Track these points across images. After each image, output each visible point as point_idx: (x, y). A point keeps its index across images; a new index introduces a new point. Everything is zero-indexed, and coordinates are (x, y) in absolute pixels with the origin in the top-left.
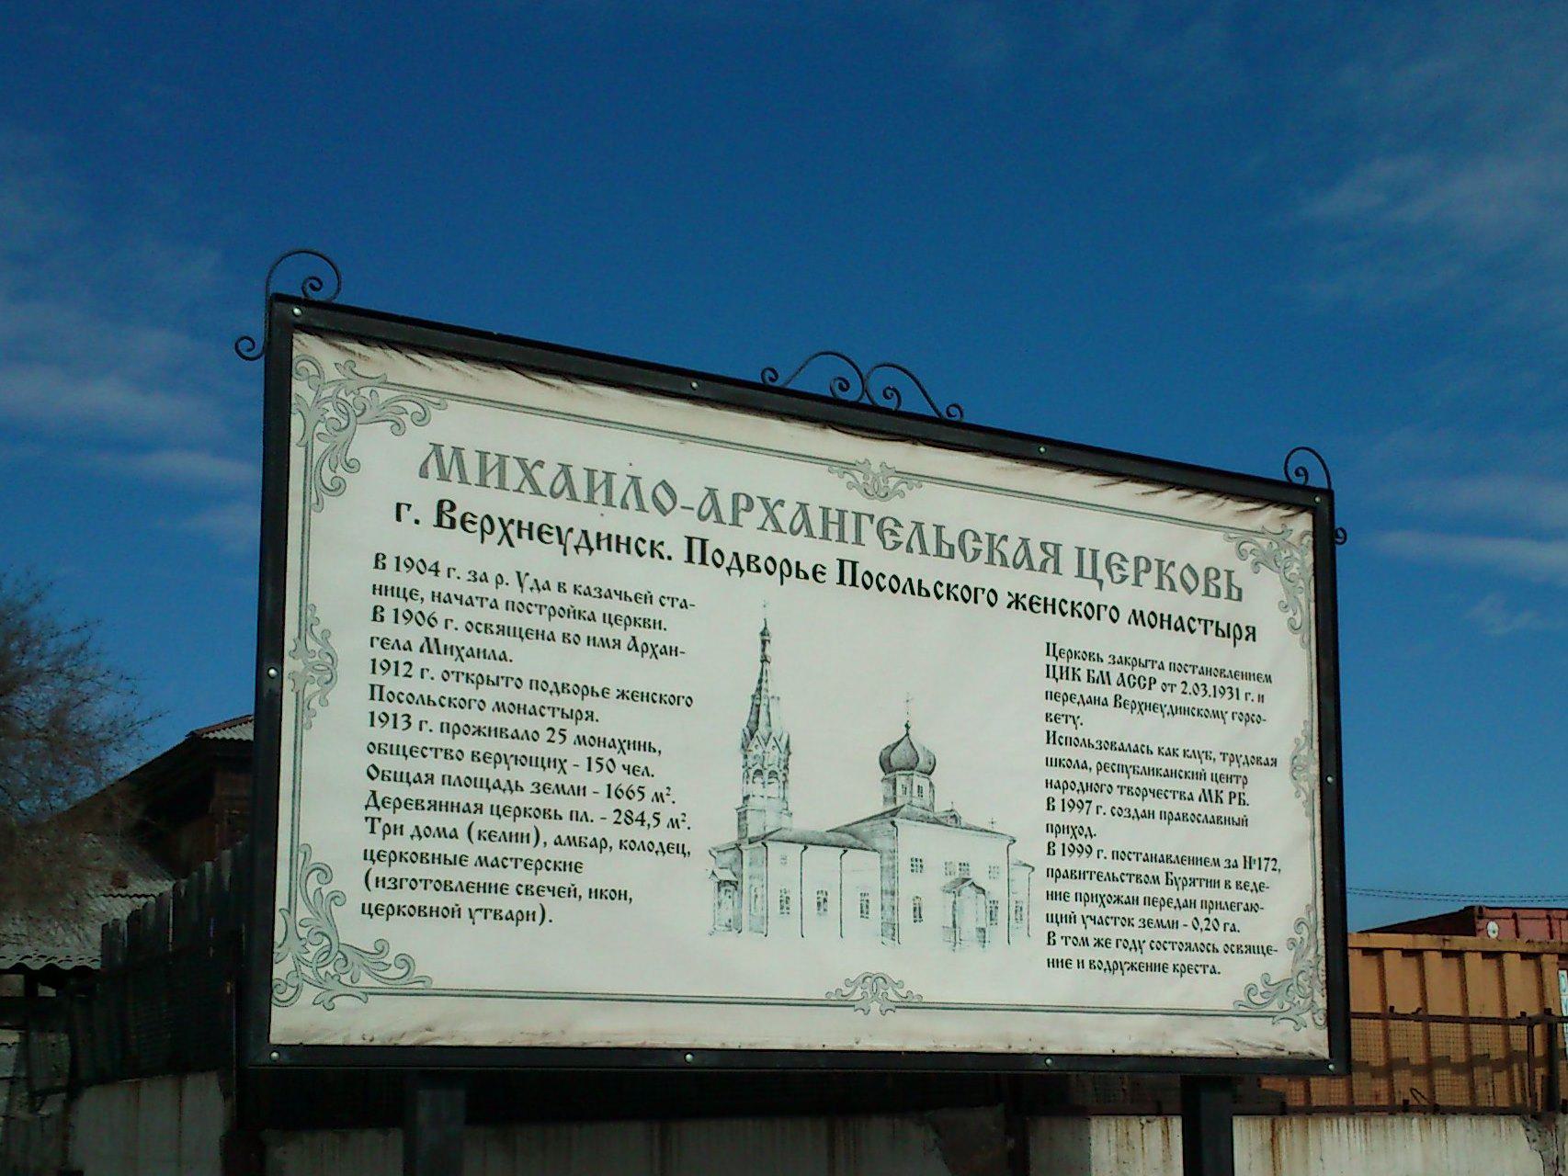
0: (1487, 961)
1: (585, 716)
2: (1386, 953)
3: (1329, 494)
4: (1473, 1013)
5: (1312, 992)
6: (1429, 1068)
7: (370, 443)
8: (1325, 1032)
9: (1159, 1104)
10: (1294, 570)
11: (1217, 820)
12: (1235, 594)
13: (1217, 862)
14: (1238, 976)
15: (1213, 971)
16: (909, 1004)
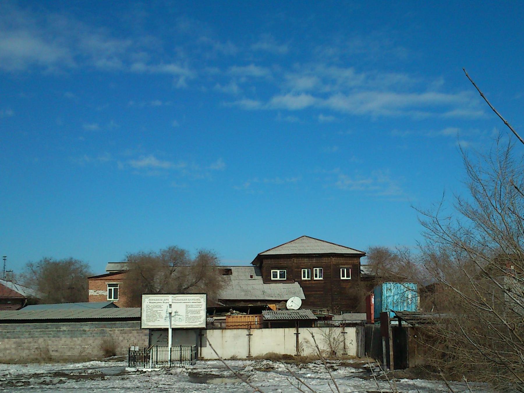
7: (146, 299)
16: (176, 325)
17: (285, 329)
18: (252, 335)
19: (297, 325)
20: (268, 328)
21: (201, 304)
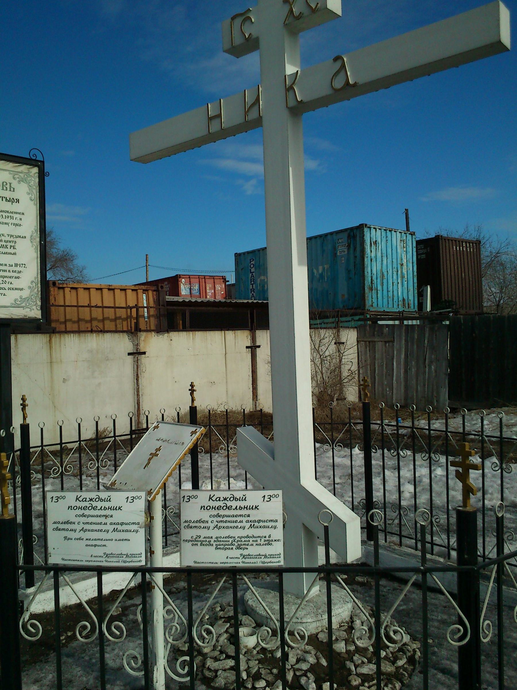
0: (133, 292)
1: (15, 201)
2: (91, 289)
3: (43, 162)
4: (117, 305)
5: (36, 301)
6: (92, 320)
8: (40, 311)
9: (14, 332)
10: (32, 183)
11: (6, 253)
12: (12, 190)
13: (6, 265)
14: (12, 296)
15: (4, 295)
17: (227, 332)
18: (144, 353)
19: (252, 322)
20: (310, 318)
21: (15, 207)
